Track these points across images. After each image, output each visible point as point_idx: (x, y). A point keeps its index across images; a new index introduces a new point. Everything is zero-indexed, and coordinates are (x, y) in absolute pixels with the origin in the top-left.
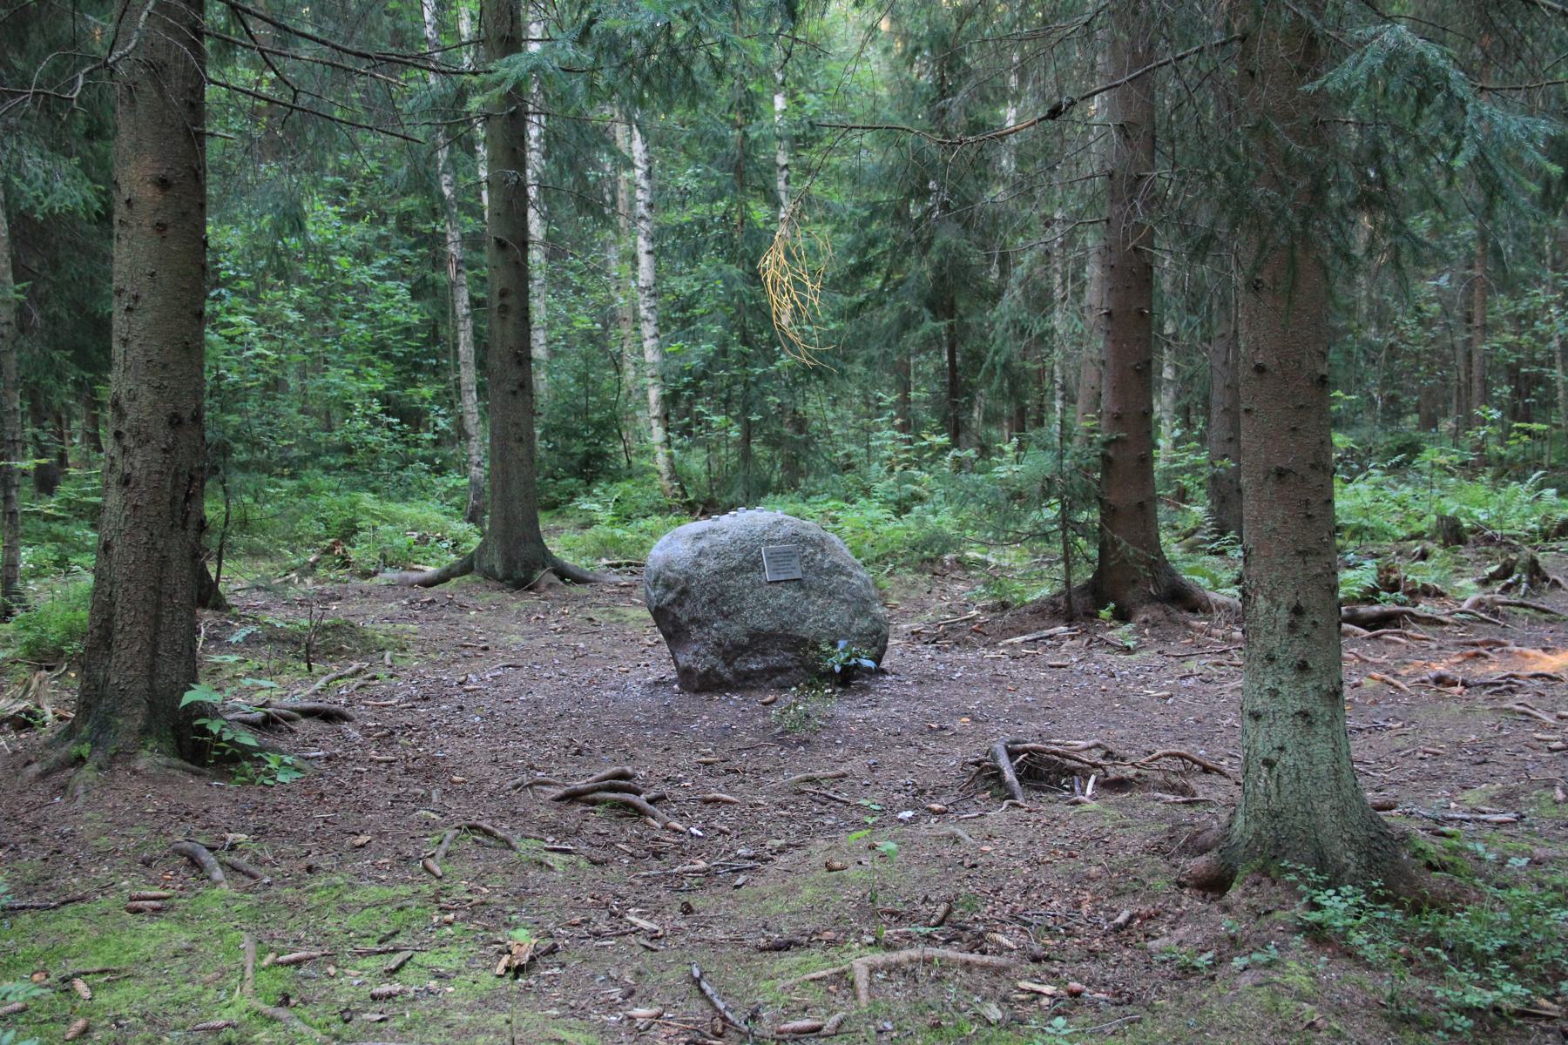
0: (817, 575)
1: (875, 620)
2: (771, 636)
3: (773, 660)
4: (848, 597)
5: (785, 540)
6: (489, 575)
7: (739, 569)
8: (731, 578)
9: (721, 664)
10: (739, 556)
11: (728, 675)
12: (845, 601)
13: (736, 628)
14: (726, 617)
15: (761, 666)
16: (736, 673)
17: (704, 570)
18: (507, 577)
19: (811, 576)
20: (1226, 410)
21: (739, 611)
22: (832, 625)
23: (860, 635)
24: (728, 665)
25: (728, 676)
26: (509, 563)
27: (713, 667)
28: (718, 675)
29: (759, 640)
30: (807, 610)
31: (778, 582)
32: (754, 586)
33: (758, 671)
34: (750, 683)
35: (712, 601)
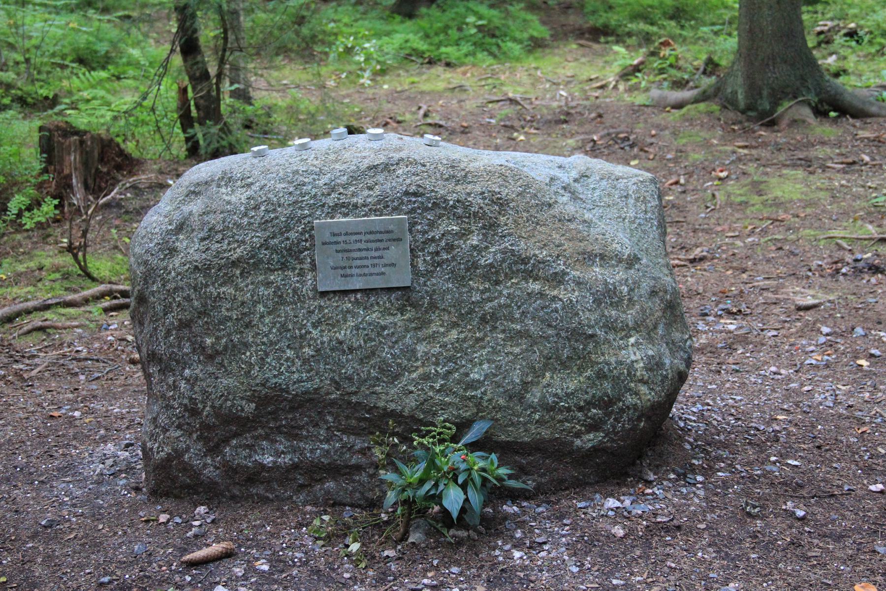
0: (459, 279)
1: (601, 375)
2: (310, 403)
3: (317, 449)
4: (533, 327)
5: (383, 205)
6: (729, 103)
7: (249, 265)
8: (229, 280)
9: (197, 447)
10: (256, 238)
11: (210, 471)
12: (524, 334)
13: (226, 381)
14: (211, 358)
15: (286, 460)
16: (230, 470)
17: (177, 261)
18: (750, 108)
19: (441, 282)
20: (678, 8)
21: (235, 349)
22: (473, 385)
23: (551, 409)
24: (214, 450)
25: (210, 472)
26: (753, 89)
27: (178, 454)
28: (186, 468)
29: (277, 410)
30: (411, 353)
31: (345, 293)
32: (280, 299)
33: (276, 467)
34: (260, 490)
35: (185, 325)
